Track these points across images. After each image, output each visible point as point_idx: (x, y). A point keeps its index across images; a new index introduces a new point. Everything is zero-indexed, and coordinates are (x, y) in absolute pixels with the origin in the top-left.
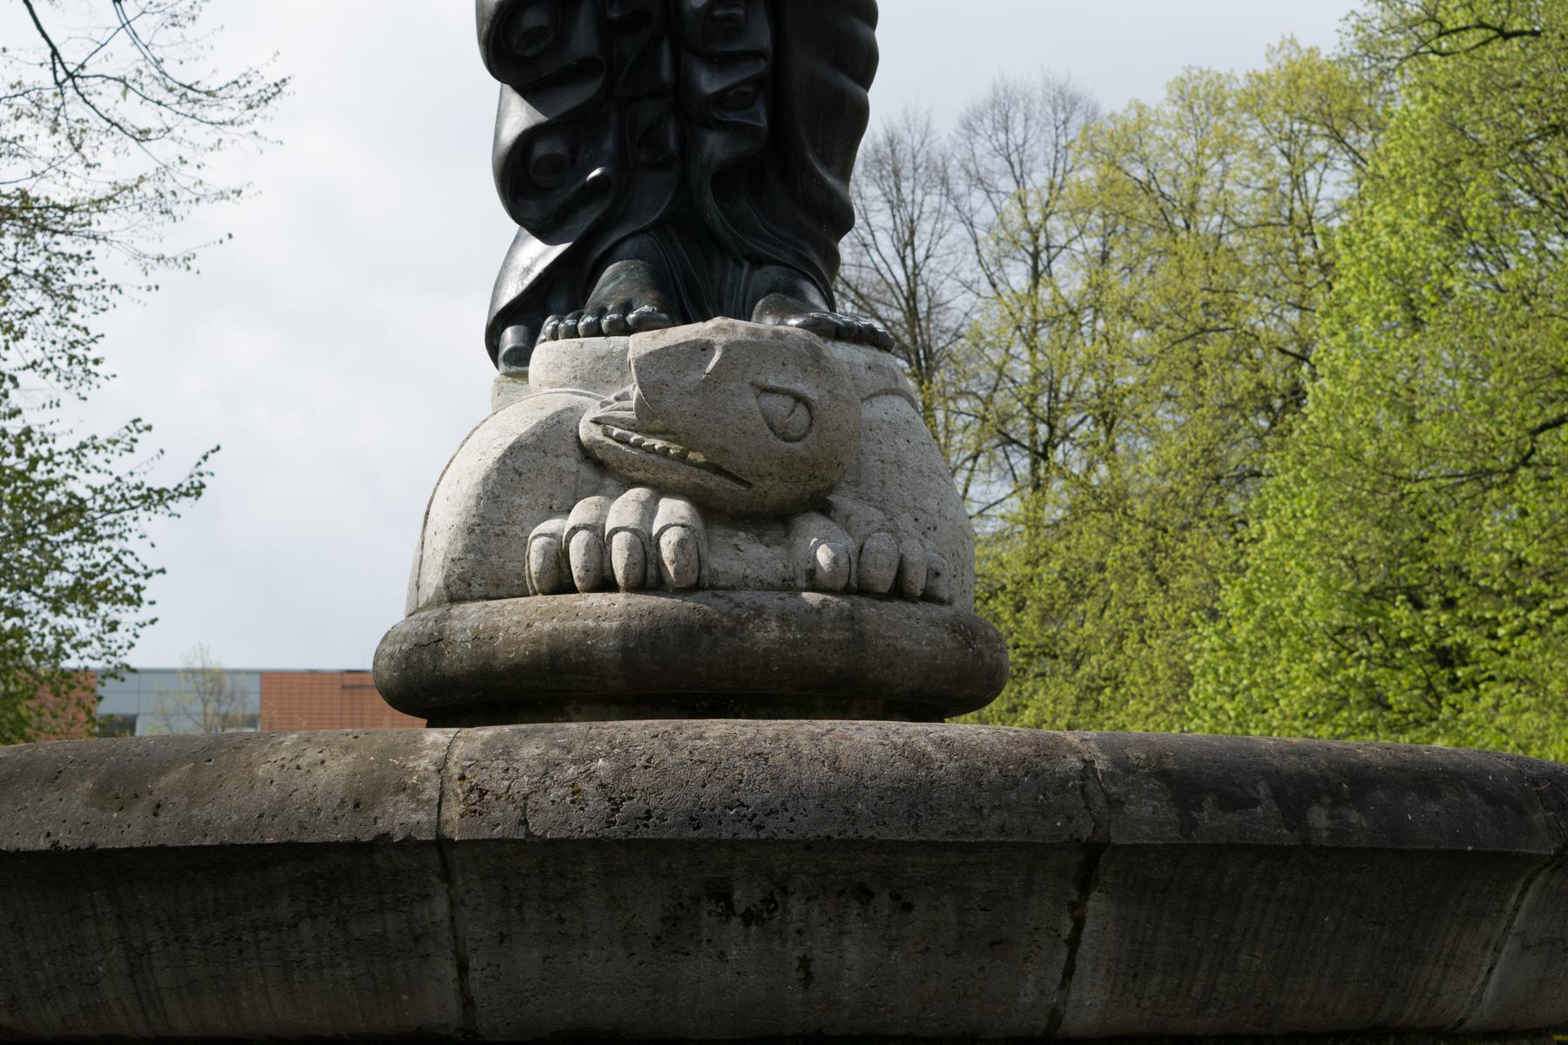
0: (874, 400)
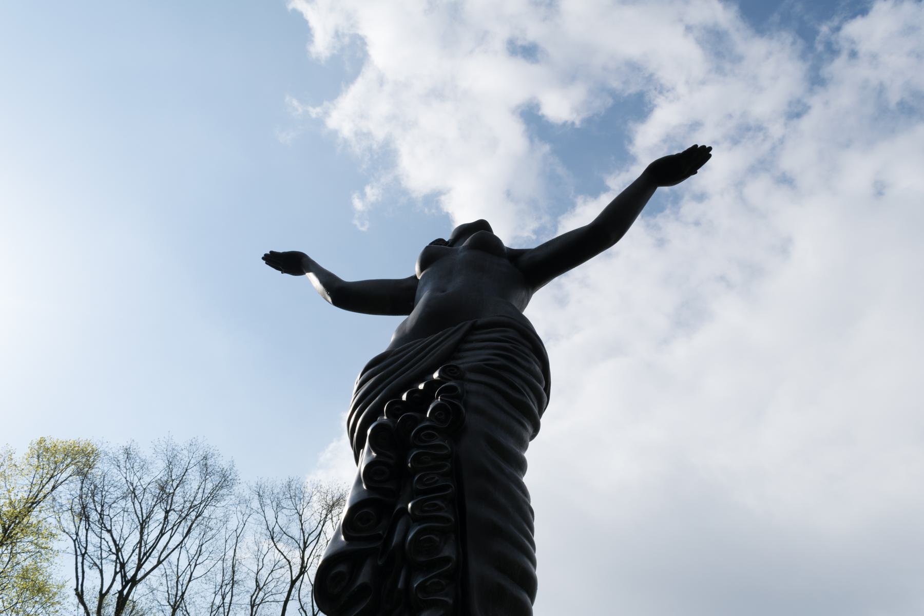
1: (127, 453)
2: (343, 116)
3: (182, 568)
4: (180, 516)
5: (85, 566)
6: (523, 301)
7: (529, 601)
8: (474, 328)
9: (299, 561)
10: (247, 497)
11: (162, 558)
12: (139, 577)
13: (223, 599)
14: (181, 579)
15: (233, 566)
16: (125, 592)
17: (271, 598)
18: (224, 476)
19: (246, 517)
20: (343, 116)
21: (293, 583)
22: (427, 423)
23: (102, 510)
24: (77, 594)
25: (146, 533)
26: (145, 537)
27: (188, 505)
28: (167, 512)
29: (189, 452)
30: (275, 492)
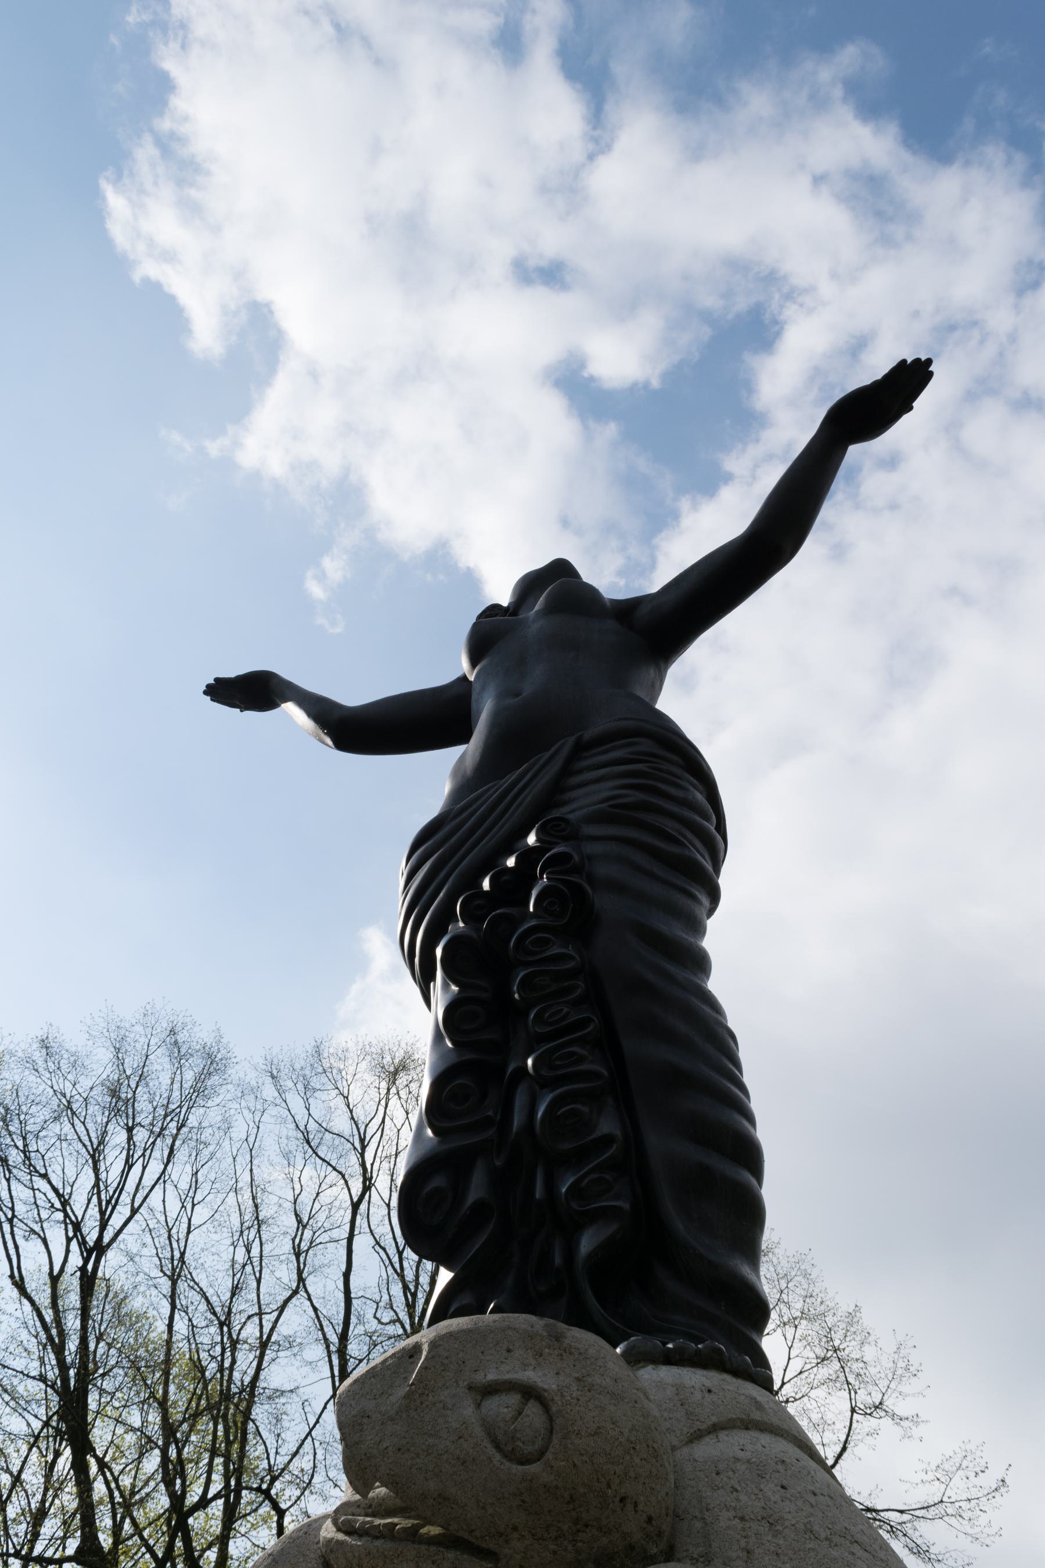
0: (722, 1435)
1: (45, 1045)
2: (274, 438)
3: (172, 1214)
4: (152, 1132)
5: (17, 1238)
6: (653, 685)
7: (754, 1182)
8: (581, 749)
9: (359, 1170)
10: (253, 1083)
11: (136, 1205)
12: (106, 1239)
13: (249, 1252)
14: (174, 1231)
15: (254, 1198)
16: (90, 1267)
17: (324, 1238)
18: (209, 1056)
19: (258, 1115)
20: (274, 438)
21: (355, 1207)
22: (533, 923)
23: (26, 1145)
24: (15, 1284)
25: (102, 1168)
26: (103, 1176)
27: (161, 1112)
28: (130, 1130)
29: (145, 1027)
30: (297, 1066)
